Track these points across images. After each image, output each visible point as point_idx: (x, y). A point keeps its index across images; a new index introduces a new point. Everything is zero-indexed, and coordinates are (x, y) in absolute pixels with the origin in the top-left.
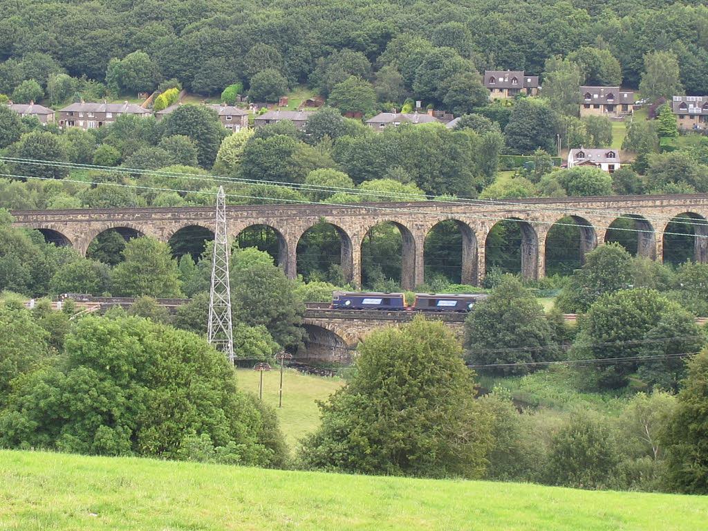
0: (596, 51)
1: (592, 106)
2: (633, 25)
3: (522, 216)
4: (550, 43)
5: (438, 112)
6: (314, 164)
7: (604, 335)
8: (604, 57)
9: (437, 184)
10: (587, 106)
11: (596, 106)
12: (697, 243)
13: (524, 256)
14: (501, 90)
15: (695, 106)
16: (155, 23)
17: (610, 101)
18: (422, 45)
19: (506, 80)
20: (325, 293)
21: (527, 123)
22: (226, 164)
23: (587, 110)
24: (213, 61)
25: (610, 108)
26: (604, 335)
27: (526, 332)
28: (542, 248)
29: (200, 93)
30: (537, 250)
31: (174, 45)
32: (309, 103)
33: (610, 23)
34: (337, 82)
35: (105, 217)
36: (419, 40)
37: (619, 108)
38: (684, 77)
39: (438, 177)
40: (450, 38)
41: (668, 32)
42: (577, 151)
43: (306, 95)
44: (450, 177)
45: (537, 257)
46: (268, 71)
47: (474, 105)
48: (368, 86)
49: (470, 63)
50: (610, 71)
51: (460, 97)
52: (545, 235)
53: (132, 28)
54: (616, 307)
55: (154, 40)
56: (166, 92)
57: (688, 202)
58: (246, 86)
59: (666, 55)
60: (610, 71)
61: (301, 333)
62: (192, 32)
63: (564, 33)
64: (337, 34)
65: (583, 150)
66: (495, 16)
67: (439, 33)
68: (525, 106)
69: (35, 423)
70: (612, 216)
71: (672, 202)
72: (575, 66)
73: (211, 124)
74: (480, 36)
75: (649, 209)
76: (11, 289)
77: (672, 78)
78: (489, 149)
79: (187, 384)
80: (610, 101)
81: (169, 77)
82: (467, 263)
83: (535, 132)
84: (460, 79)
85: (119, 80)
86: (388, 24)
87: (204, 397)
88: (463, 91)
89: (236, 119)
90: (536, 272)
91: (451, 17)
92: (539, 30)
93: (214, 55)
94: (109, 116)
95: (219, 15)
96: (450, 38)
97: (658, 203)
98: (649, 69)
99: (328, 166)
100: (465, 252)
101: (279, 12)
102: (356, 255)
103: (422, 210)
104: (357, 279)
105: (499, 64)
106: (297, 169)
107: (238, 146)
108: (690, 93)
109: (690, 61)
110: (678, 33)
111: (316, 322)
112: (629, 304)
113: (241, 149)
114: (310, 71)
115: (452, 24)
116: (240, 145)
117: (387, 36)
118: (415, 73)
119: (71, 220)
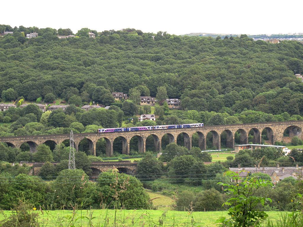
0: (143, 87)
1: (143, 102)
2: (152, 79)
3: (139, 135)
4: (129, 84)
5: (100, 105)
6: (72, 121)
7: (179, 168)
8: (145, 88)
9: (107, 125)
10: (142, 102)
11: (145, 102)
12: (185, 141)
13: (139, 146)
15: (172, 102)
16: (15, 80)
17: (149, 101)
20: (94, 159)
21: (128, 107)
22: (44, 121)
23: (142, 103)
24: (33, 91)
25: (149, 102)
26: (179, 168)
27: (155, 168)
28: (145, 144)
29: (30, 100)
30: (143, 144)
31: (21, 86)
32: (62, 103)
33: (145, 78)
34: (70, 96)
35: (24, 138)
36: (92, 84)
37: (151, 102)
38: (168, 93)
39: (107, 124)
41: (162, 81)
42: (143, 115)
43: (61, 100)
44: (110, 123)
45: (143, 146)
46: (50, 94)
47: (111, 102)
48: (79, 97)
49: (108, 90)
51: (107, 100)
52: (145, 140)
53: (8, 82)
54: (181, 160)
55: (15, 85)
56: (20, 100)
58: (43, 98)
59: (163, 87)
61: (91, 170)
62: (26, 82)
64: (68, 82)
65: (145, 115)
66: (113, 77)
67: (98, 82)
68: (126, 102)
69: (94, 201)
72: (138, 91)
73: (38, 109)
76: (3, 160)
77: (165, 94)
78: (120, 116)
79: (133, 189)
80: (149, 101)
81: (21, 96)
82: (124, 148)
83: (130, 110)
84: (107, 95)
85: (6, 97)
86: (83, 80)
87: (137, 192)
88: (108, 99)
89: (43, 108)
90: (143, 150)
91: (100, 77)
92: (126, 81)
93: (33, 89)
94: (5, 107)
95: (33, 77)
96: (101, 83)
98: (159, 91)
99: (76, 121)
100: (123, 145)
101: (51, 76)
102: (95, 147)
103: (112, 134)
104: (95, 154)
106: (67, 122)
107: (47, 116)
108: (170, 98)
109: (169, 89)
110: (165, 81)
111: (95, 167)
112: (185, 160)
113: (48, 117)
114: (61, 94)
115: (101, 79)
116: (48, 115)
117: (83, 83)
118: (92, 94)
119: (15, 140)
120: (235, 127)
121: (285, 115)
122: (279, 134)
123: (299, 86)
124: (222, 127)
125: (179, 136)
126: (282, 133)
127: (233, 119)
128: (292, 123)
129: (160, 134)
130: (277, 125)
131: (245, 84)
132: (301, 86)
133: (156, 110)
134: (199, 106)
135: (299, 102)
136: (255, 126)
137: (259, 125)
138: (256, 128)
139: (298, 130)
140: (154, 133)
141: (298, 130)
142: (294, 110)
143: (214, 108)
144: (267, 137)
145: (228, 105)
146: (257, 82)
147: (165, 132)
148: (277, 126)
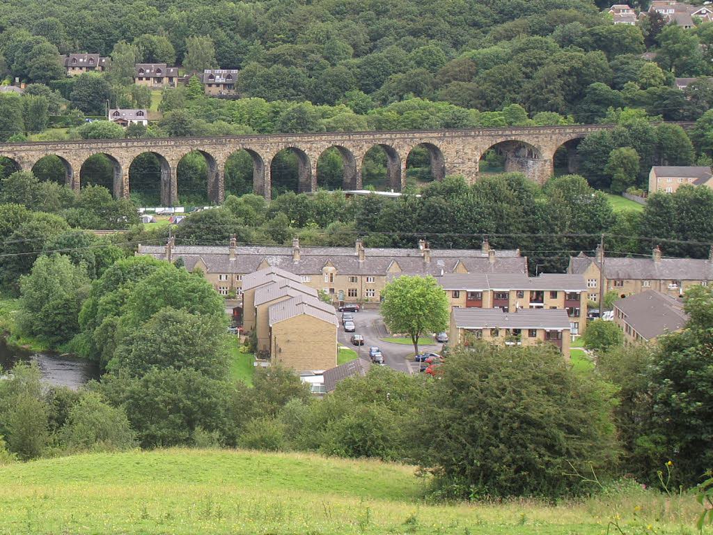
0: (155, 38)
1: (144, 79)
3: (10, 156)
4: (123, 33)
10: (141, 79)
11: (148, 79)
14: (81, 68)
15: (220, 77)
17: (158, 75)
18: (24, 35)
19: (85, 61)
23: (141, 81)
25: (159, 80)
37: (166, 80)
40: (46, 30)
50: (165, 53)
57: (149, 144)
60: (165, 53)
63: (135, 24)
65: (119, 110)
66: (85, 13)
67: (38, 26)
70: (85, 156)
71: (135, 144)
74: (70, 28)
75: (117, 149)
80: (158, 75)
91: (51, 14)
96: (46, 30)
97: (124, 144)
105: (85, 49)
120: (317, 139)
121: (512, 113)
122: (463, 163)
123: (593, 34)
124: (276, 140)
125: (137, 164)
126: (475, 162)
127: (347, 122)
128: (507, 133)
129: (76, 155)
130: (459, 137)
131: (437, 28)
132: (597, 34)
133: (164, 99)
134: (282, 89)
135: (566, 77)
136: (385, 138)
137: (398, 136)
138: (387, 144)
139: (530, 154)
140: (56, 150)
141: (530, 154)
142: (547, 99)
143: (326, 93)
144: (430, 172)
145: (367, 85)
146: (476, 24)
147: (91, 149)
148: (458, 140)
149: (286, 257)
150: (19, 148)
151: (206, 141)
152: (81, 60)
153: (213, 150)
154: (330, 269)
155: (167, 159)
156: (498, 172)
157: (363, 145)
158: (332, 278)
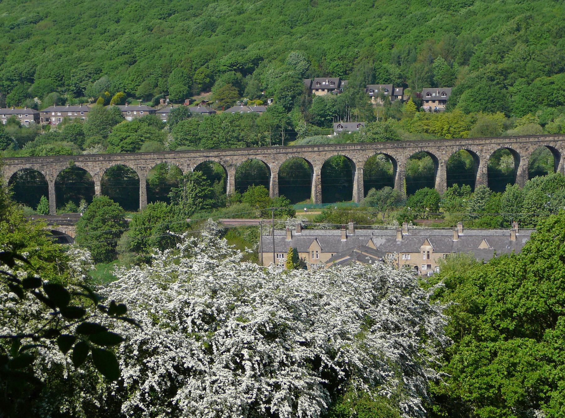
147: (287, 153)
149: (390, 237)
150: (224, 153)
151: (389, 145)
152: (324, 83)
153: (394, 153)
154: (428, 247)
155: (354, 161)
156: (208, 92)
157: (529, 147)
158: (428, 255)
